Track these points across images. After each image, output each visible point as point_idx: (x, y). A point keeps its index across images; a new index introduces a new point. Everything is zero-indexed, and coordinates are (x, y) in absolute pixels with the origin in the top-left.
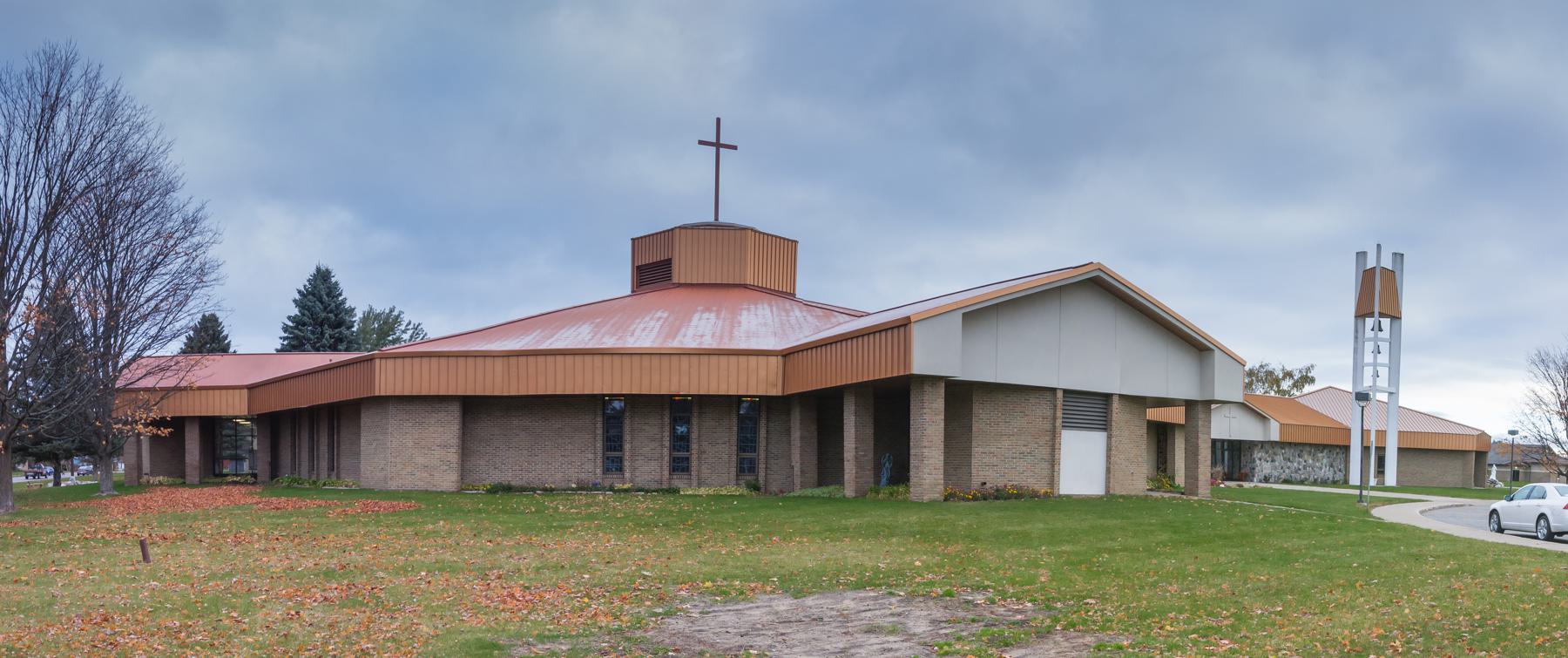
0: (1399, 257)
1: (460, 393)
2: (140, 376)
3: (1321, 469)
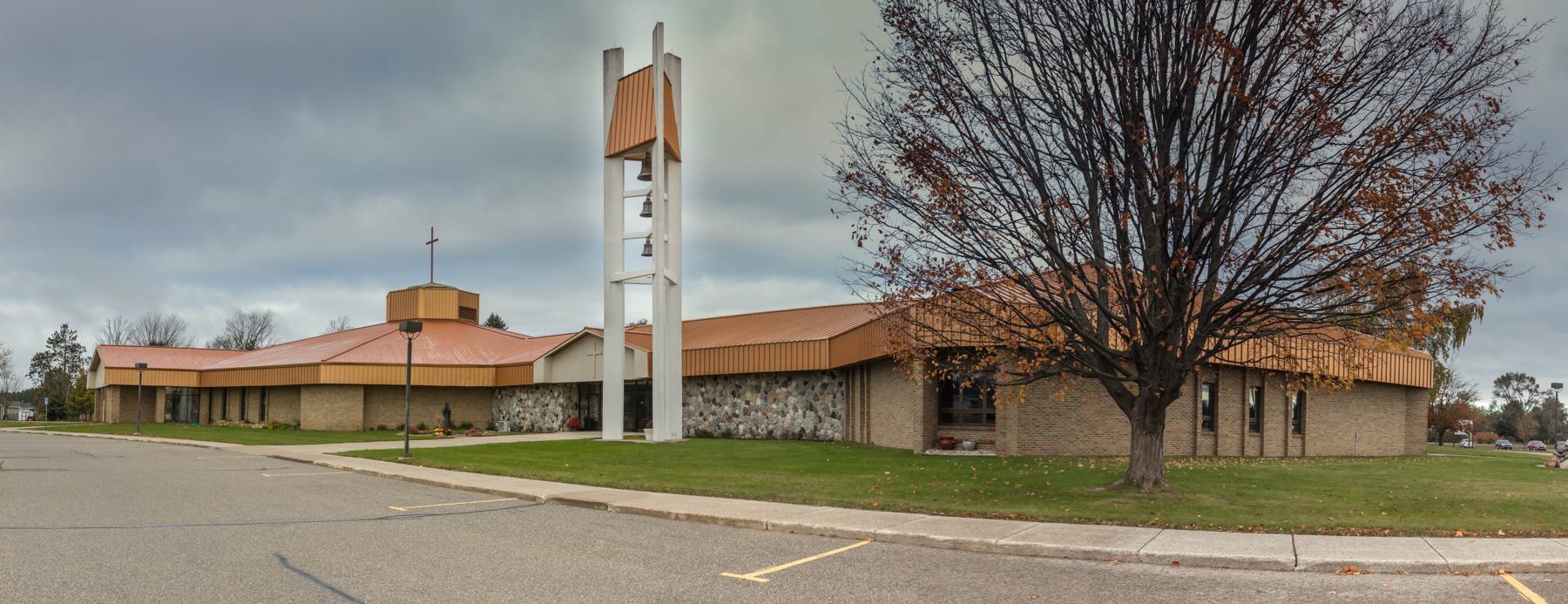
0: (673, 63)
1: (365, 383)
3: (784, 414)
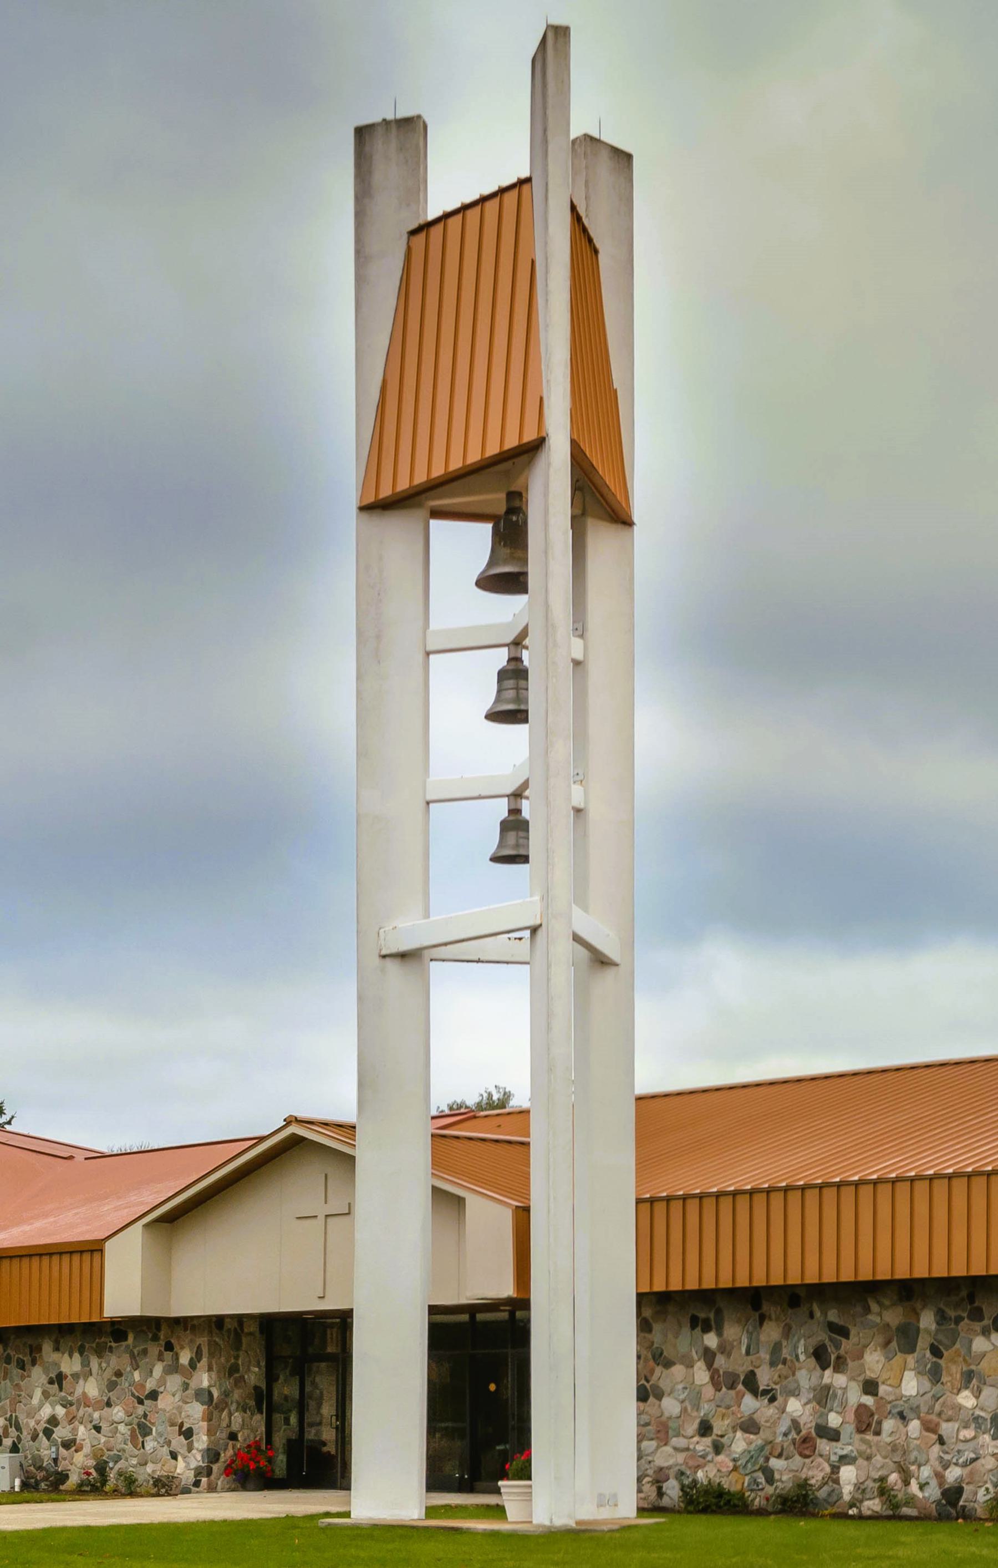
2: (38, 1285)
